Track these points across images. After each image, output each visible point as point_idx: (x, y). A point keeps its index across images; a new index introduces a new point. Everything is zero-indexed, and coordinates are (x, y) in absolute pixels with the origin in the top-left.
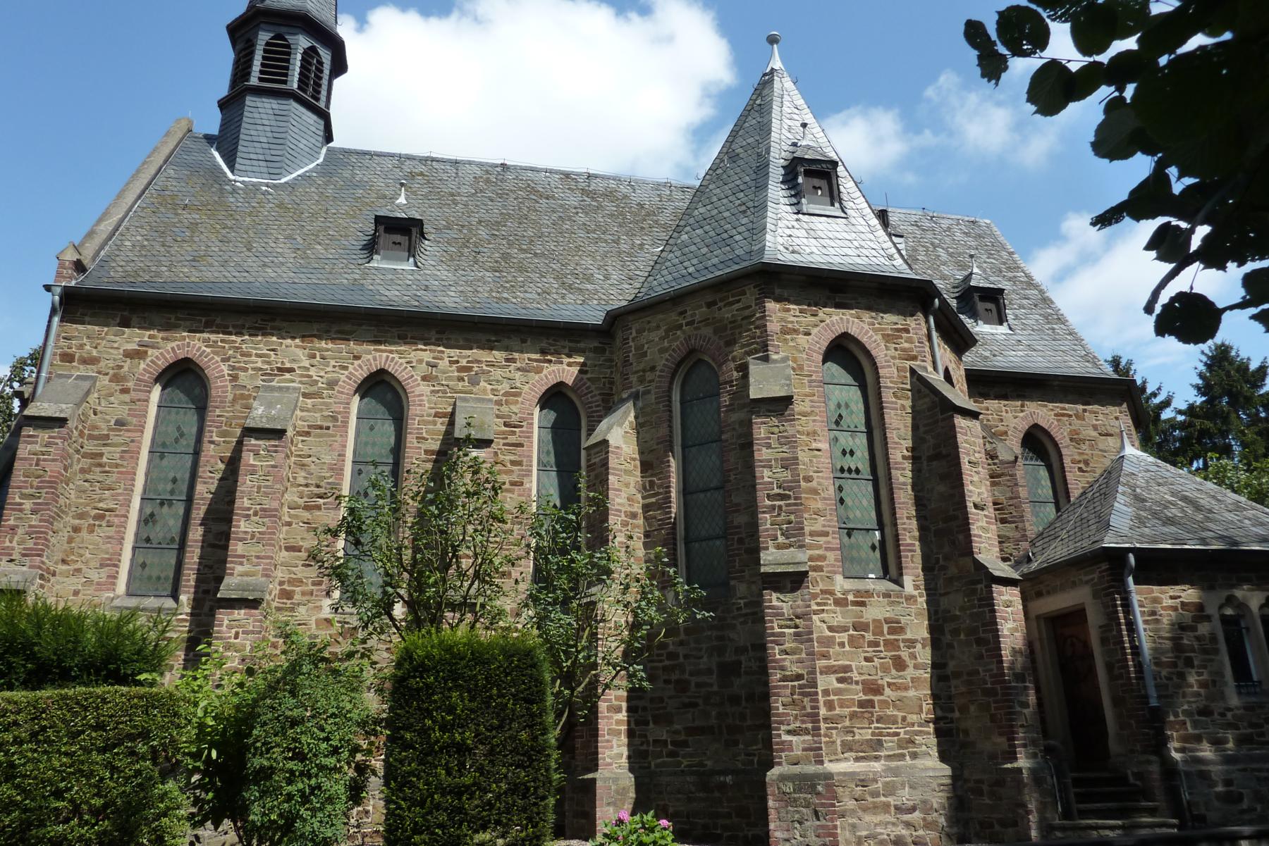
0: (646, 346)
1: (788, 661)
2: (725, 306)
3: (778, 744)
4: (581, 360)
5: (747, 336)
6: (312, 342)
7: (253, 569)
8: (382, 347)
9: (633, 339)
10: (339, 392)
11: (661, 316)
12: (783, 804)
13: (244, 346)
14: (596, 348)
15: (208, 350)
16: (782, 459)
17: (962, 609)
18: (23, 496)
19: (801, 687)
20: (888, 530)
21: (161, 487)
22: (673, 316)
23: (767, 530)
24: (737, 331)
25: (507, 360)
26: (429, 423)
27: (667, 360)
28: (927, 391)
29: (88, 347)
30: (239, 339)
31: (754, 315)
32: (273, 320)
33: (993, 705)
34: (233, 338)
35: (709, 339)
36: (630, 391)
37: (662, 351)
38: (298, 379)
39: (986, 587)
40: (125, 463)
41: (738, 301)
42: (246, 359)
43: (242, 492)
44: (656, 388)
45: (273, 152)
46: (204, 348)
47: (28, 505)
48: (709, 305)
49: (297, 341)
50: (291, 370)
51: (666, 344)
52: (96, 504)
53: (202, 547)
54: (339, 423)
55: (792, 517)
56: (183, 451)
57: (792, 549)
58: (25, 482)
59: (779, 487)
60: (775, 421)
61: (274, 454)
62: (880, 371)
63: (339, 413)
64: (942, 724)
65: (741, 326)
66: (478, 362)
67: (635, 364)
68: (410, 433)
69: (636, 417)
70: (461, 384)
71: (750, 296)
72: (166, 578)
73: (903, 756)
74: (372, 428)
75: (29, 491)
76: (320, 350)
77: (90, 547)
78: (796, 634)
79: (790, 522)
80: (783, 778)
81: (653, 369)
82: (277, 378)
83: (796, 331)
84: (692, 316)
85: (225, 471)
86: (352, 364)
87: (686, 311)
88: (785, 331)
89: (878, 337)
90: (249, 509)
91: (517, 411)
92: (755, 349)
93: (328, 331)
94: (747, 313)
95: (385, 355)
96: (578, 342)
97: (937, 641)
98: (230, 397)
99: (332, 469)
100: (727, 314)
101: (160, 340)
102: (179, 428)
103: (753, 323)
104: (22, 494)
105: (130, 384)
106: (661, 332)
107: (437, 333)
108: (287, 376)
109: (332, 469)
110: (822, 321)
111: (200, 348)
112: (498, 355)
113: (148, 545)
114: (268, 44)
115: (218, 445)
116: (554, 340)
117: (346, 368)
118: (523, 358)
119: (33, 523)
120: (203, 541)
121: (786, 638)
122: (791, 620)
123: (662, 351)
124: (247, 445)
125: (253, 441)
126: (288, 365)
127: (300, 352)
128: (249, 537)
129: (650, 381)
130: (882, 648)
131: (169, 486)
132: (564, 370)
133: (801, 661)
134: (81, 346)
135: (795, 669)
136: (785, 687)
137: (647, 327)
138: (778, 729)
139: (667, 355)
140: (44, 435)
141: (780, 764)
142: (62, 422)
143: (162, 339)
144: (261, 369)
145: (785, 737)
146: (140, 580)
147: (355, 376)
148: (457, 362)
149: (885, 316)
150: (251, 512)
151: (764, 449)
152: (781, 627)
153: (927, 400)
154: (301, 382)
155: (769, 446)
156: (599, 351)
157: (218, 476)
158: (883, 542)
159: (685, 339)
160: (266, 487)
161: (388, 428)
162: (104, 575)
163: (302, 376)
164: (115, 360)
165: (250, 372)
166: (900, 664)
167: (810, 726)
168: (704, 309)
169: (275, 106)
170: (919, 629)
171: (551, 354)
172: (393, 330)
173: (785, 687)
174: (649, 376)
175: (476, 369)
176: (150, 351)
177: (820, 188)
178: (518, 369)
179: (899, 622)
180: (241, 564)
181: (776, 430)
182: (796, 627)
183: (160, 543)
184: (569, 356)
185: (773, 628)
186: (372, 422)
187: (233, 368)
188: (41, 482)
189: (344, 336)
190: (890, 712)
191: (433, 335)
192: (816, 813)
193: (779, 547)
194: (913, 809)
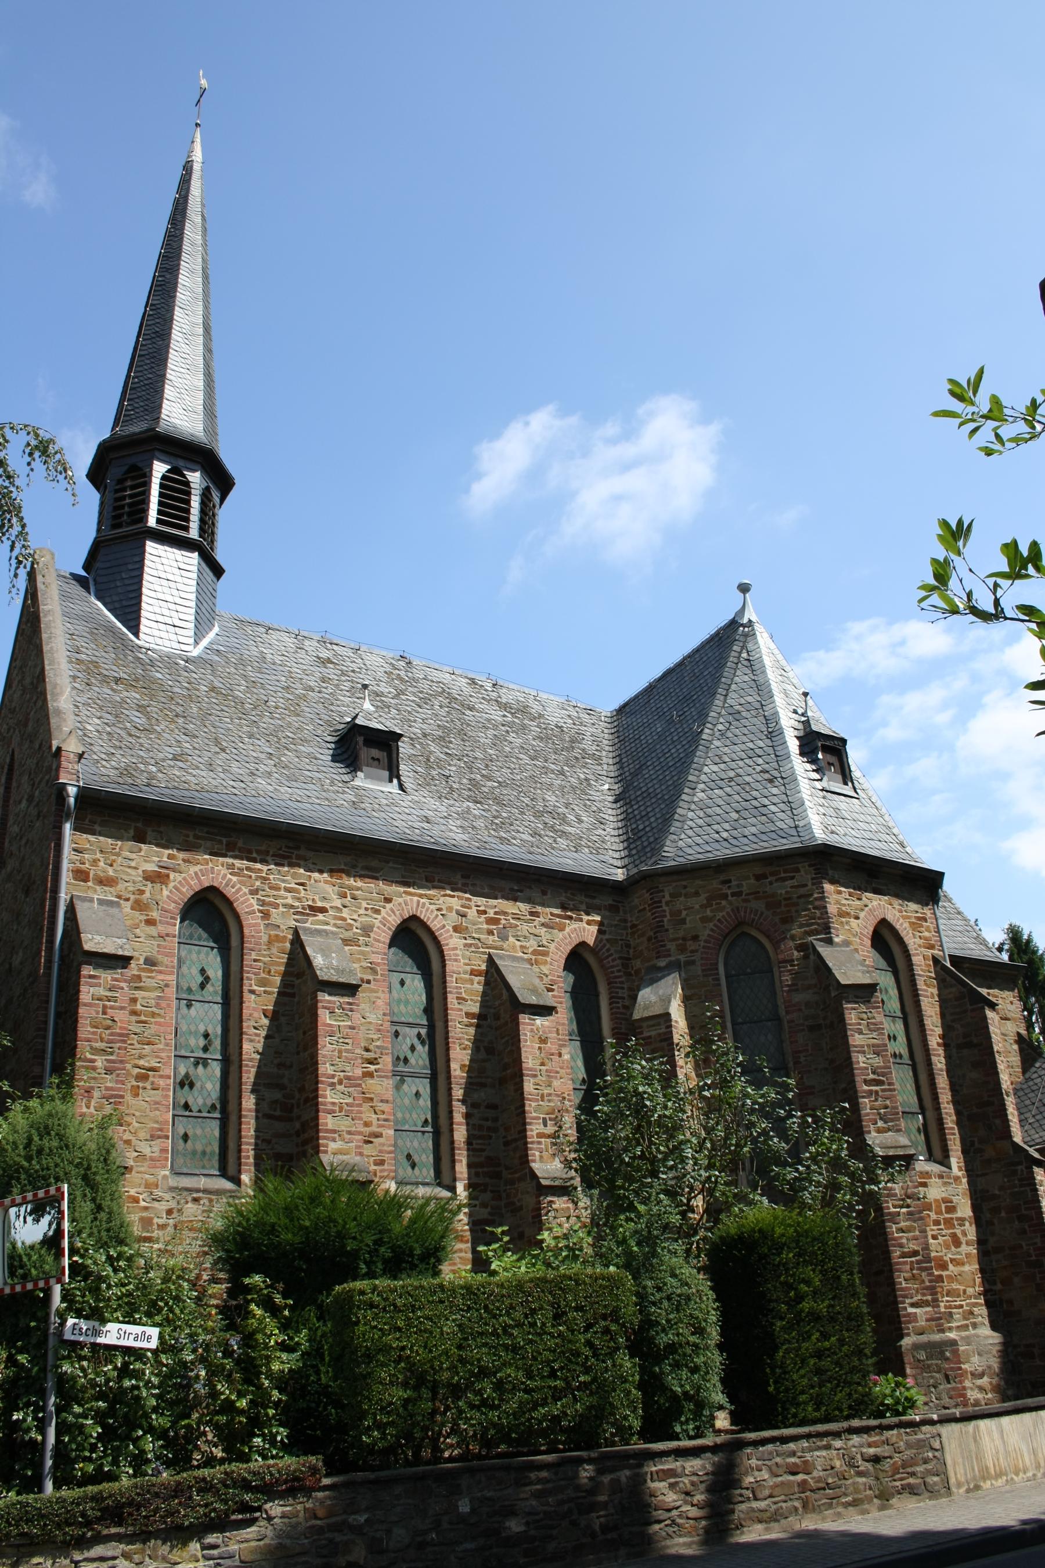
0: (684, 913)
1: (904, 1239)
2: (776, 880)
3: (905, 1316)
4: (598, 918)
5: (805, 916)
6: (341, 878)
7: (345, 1146)
8: (411, 890)
9: (667, 904)
10: (376, 940)
11: (699, 882)
12: (918, 1371)
13: (271, 877)
14: (610, 905)
15: (235, 879)
16: (874, 1046)
17: (1001, 1188)
18: (95, 1051)
19: (918, 1262)
20: (930, 1114)
21: (192, 1042)
22: (715, 884)
23: (868, 1114)
24: (793, 909)
25: (532, 914)
26: (465, 981)
27: (712, 930)
28: (954, 982)
29: (102, 864)
30: (265, 868)
31: (812, 895)
32: (298, 848)
33: (1038, 1276)
34: (258, 866)
35: (762, 913)
36: (668, 960)
37: (705, 920)
38: (332, 922)
39: (1027, 1168)
40: (162, 1012)
41: (792, 878)
42: (275, 893)
43: (324, 1056)
44: (702, 958)
45: (182, 616)
46: (229, 876)
47: (100, 1062)
48: (758, 878)
49: (325, 875)
50: (323, 910)
51: (708, 913)
52: (136, 1062)
53: (257, 1118)
54: (379, 977)
55: (888, 1102)
56: (210, 998)
57: (890, 1133)
58: (94, 1033)
59: (874, 1073)
60: (863, 1008)
61: (350, 1013)
62: (913, 958)
63: (378, 964)
64: (989, 1297)
65: (796, 904)
66: (505, 913)
67: (671, 931)
68: (450, 992)
69: (683, 989)
70: (491, 937)
71: (805, 873)
72: (212, 1153)
73: (967, 1326)
74: (402, 983)
75: (99, 1045)
76: (350, 888)
77: (137, 1114)
78: (909, 1213)
79: (886, 1107)
80: (916, 1347)
81: (695, 938)
82: (311, 919)
83: (848, 914)
84: (738, 886)
85: (269, 1028)
86: (384, 907)
87: (730, 881)
88: (842, 914)
89: (906, 925)
90: (333, 1076)
91: (547, 972)
92: (816, 929)
93: (354, 867)
94: (802, 891)
95: (416, 899)
96: (594, 898)
97: (978, 1219)
98: (265, 939)
99: (379, 1030)
100: (781, 889)
101: (180, 862)
102: (203, 971)
103: (811, 903)
104: (92, 1048)
105: (155, 915)
106: (702, 898)
107: (463, 877)
108: (320, 917)
109: (379, 1030)
110: (866, 906)
111: (225, 876)
112: (523, 907)
113: (187, 1113)
114: (164, 477)
115: (259, 995)
116: (572, 894)
117: (377, 912)
118: (547, 912)
119: (109, 1085)
120: (257, 1111)
121: (901, 1217)
122: (903, 1200)
123: (705, 920)
124: (321, 1001)
125: (327, 997)
126: (319, 904)
127: (329, 889)
128: (337, 1108)
129: (692, 951)
130: (942, 1227)
131: (202, 1042)
132: (584, 929)
133: (915, 1238)
134: (95, 862)
135: (913, 1246)
136: (905, 1263)
137: (683, 891)
138: (904, 1303)
139: (711, 924)
140: (106, 976)
141: (908, 1335)
142: (122, 961)
143: (184, 860)
144: (292, 907)
145: (911, 1310)
146: (184, 1155)
147: (389, 922)
148: (485, 912)
149: (909, 904)
150: (335, 1080)
151: (856, 1035)
152: (895, 1207)
153: (954, 990)
154: (335, 925)
155: (861, 1033)
156: (613, 909)
157: (264, 1033)
158: (925, 1125)
159: (733, 910)
160: (347, 1051)
161: (416, 984)
162: (156, 1149)
163: (336, 918)
164: (134, 882)
165: (281, 909)
166: (957, 1243)
167: (929, 1298)
168: (752, 881)
169: (180, 558)
170: (965, 1210)
171: (571, 910)
172: (421, 871)
173: (905, 1263)
174: (691, 945)
175: (503, 922)
176: (172, 875)
177: (832, 764)
178: (543, 925)
179: (951, 1202)
180: (334, 1140)
181: (865, 1016)
182: (908, 1206)
183: (200, 1111)
184: (588, 914)
185: (888, 1208)
186: (403, 976)
187: (263, 903)
188: (112, 1034)
189: (371, 873)
190: (955, 1286)
191: (458, 878)
192: (947, 1377)
193: (879, 1131)
194: (981, 1376)
